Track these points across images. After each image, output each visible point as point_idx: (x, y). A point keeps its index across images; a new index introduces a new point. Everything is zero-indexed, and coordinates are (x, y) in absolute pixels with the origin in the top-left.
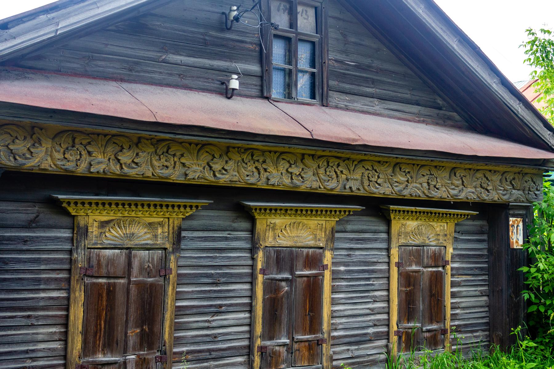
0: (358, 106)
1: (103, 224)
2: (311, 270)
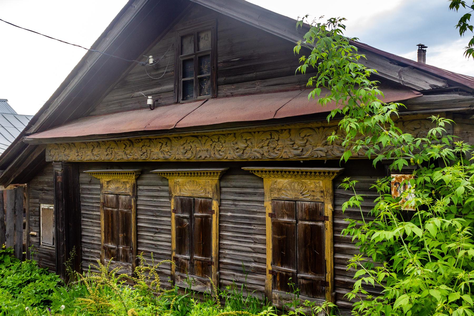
0: (241, 90)
1: (108, 182)
2: (203, 213)
